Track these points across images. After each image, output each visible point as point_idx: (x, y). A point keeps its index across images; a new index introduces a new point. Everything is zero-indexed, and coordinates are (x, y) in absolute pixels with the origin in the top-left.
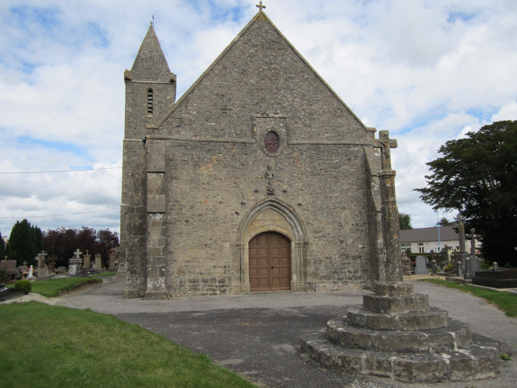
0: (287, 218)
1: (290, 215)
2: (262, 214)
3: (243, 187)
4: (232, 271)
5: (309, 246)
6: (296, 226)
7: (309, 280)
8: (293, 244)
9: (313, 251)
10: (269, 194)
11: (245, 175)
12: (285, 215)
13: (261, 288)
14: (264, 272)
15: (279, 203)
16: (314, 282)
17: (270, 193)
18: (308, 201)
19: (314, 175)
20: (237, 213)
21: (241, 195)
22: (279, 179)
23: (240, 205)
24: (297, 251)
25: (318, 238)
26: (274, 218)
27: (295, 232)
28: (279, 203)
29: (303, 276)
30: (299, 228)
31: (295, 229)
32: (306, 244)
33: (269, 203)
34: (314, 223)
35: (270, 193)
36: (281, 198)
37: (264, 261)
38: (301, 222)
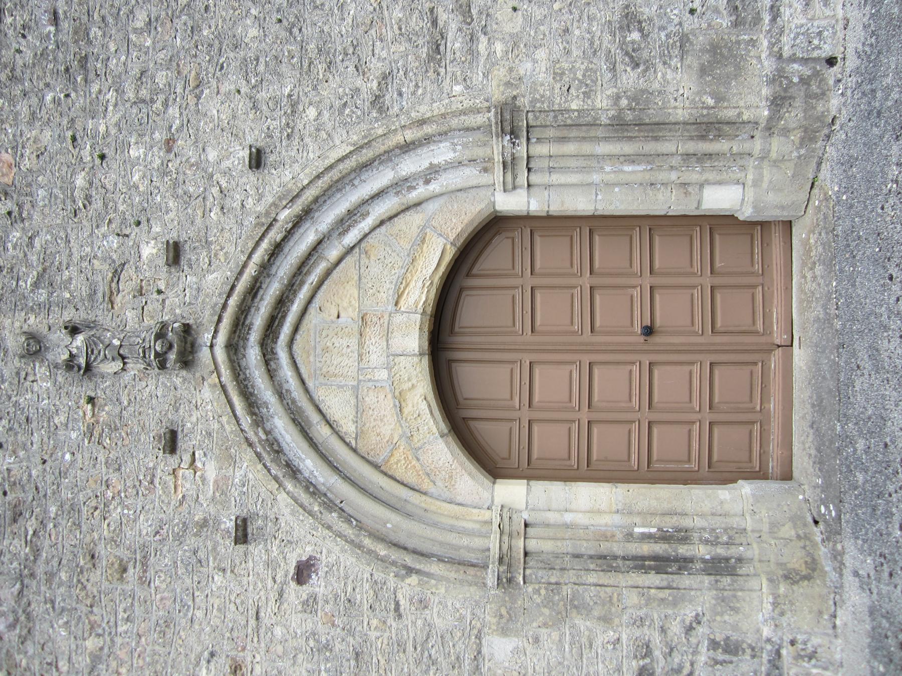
0: (351, 238)
1: (327, 219)
2: (320, 394)
3: (145, 526)
4: (676, 629)
5: (524, 102)
6: (401, 185)
7: (752, 100)
8: (510, 203)
9: (558, 75)
10: (187, 360)
11: (74, 508)
12: (333, 253)
13: (774, 406)
14: (670, 383)
15: (254, 291)
16: (769, 65)
17: (178, 348)
18: (241, 105)
19: (84, 61)
20: (303, 572)
21: (191, 542)
22: (102, 288)
23: (256, 550)
24: (556, 178)
25: (472, 38)
26: (350, 315)
27: (434, 187)
28: (254, 291)
29: (722, 146)
30: (409, 165)
31: (421, 191)
32: (510, 122)
33: (253, 354)
34: (376, 67)
35: (178, 348)
36: (216, 280)
37: (611, 384)
38: (367, 154)
